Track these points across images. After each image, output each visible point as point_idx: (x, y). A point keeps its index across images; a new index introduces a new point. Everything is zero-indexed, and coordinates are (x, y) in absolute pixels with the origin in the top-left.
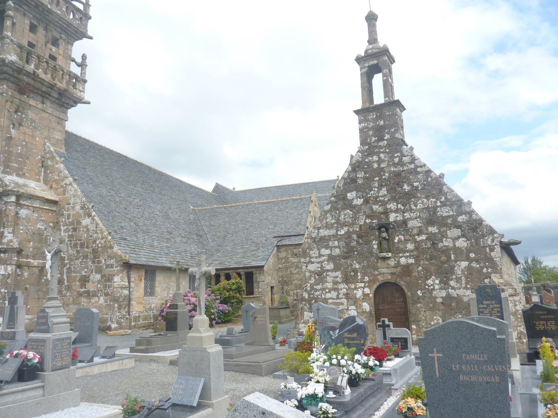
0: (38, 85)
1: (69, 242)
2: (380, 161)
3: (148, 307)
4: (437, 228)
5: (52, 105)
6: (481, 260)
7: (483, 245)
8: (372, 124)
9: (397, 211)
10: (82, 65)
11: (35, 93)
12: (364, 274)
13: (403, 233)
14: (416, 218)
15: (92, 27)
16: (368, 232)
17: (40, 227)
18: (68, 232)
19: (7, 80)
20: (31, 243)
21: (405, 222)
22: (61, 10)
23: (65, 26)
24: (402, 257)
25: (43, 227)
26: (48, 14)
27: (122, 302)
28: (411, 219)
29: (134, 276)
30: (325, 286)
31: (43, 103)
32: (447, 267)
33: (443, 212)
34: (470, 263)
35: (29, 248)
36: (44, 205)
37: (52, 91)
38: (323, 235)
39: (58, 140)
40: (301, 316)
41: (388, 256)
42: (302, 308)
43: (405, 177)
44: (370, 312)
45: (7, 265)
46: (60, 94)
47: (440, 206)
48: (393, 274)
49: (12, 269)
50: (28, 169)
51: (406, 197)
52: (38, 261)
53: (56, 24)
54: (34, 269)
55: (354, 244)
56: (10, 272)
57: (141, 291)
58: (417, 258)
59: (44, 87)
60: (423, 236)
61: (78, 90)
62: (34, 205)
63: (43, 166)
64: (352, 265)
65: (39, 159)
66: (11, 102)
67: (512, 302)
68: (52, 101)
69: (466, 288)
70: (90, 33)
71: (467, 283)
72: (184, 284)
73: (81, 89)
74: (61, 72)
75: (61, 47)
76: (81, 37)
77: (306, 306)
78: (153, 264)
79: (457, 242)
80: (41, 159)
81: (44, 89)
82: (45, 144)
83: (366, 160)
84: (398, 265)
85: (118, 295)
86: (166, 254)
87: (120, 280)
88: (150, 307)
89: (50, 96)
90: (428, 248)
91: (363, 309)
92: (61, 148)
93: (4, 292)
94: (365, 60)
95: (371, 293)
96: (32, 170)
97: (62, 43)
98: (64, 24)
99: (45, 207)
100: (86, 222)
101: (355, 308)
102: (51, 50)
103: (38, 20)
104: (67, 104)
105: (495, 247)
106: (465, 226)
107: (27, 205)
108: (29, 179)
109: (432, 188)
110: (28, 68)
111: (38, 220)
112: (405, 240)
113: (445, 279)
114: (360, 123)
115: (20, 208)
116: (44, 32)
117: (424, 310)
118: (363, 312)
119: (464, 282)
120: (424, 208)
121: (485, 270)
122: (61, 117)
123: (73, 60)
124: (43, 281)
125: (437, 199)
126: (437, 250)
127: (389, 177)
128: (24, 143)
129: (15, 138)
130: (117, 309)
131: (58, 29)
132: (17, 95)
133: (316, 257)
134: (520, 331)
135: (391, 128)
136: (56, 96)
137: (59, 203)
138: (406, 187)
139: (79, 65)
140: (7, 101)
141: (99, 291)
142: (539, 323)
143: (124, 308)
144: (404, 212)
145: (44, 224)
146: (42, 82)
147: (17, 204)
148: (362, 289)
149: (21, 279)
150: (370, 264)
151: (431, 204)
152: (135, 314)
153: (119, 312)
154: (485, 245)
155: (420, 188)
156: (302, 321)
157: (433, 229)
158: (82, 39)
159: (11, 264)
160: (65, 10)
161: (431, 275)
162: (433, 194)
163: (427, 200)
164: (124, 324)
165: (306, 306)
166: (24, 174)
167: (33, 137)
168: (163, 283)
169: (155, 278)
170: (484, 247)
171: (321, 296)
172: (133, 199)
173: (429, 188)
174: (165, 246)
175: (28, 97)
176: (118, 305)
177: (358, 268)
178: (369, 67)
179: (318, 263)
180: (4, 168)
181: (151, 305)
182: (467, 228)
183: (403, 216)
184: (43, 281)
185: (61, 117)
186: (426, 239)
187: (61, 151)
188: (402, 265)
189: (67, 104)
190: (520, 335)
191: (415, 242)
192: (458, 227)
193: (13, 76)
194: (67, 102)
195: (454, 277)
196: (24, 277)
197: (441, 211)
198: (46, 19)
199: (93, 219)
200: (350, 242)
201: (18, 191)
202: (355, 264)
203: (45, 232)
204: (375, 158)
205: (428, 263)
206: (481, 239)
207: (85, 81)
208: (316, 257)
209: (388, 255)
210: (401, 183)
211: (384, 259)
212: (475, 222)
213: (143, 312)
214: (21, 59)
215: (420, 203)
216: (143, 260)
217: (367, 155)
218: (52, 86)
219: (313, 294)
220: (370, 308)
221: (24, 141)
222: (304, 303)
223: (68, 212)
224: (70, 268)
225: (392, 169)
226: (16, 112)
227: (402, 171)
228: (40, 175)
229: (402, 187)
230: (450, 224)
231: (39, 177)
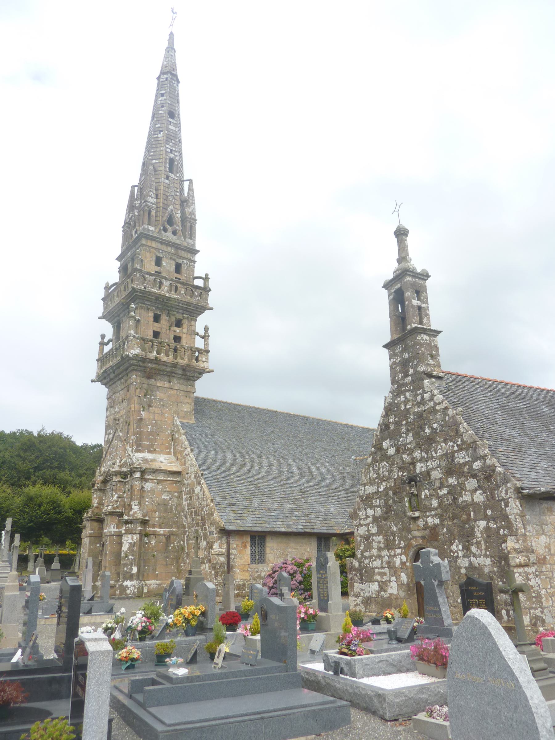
0: (163, 367)
1: (188, 511)
2: (406, 402)
3: (256, 575)
4: (456, 479)
5: (179, 381)
6: (498, 518)
7: (497, 498)
8: (399, 359)
9: (421, 460)
10: (205, 337)
11: (162, 374)
12: (401, 539)
13: (427, 487)
14: (437, 467)
15: (212, 299)
16: (400, 488)
17: (165, 498)
18: (187, 501)
19: (136, 370)
20: (157, 513)
21: (428, 473)
22: (180, 294)
23: (185, 306)
24: (428, 517)
25: (168, 497)
26: (167, 302)
27: (219, 569)
28: (433, 469)
29: (235, 543)
30: (372, 553)
31: (170, 382)
32: (468, 528)
33: (460, 459)
34: (487, 524)
35: (155, 518)
36: (168, 477)
37: (175, 369)
38: (368, 493)
39: (187, 412)
40: (351, 588)
41: (415, 516)
42: (351, 579)
43: (426, 418)
44: (408, 584)
45: (133, 534)
46: (184, 370)
47: (457, 450)
48: (423, 537)
49: (137, 538)
50: (158, 444)
51: (427, 442)
52: (164, 529)
53: (177, 307)
54: (161, 537)
55: (391, 502)
56: (136, 541)
57: (246, 558)
58: (441, 517)
59: (168, 368)
60: (445, 489)
61: (201, 362)
62: (158, 478)
63: (172, 439)
64: (391, 528)
65: (168, 433)
66: (140, 388)
67: (522, 574)
68: (179, 377)
69: (486, 556)
70: (210, 305)
71: (486, 550)
72: (308, 550)
73: (204, 359)
74: (183, 350)
75: (185, 326)
76: (202, 311)
77: (357, 576)
78: (260, 529)
79: (475, 496)
80: (171, 433)
81: (168, 369)
82: (173, 419)
83: (396, 401)
84: (426, 527)
85: (215, 562)
86: (285, 518)
87: (218, 547)
88: (260, 575)
89: (176, 374)
90: (449, 504)
91: (401, 581)
92: (191, 419)
93: (132, 559)
94: (392, 285)
95: (407, 561)
96: (163, 444)
97: (185, 322)
98: (185, 305)
99: (168, 479)
100: (197, 490)
101: (395, 580)
102: (175, 331)
103: (161, 310)
104: (193, 377)
105: (510, 500)
106: (480, 474)
107: (151, 479)
108: (160, 453)
109: (449, 429)
110: (150, 356)
111: (163, 491)
112: (430, 495)
113: (467, 544)
114: (390, 359)
115: (145, 482)
116: (167, 318)
117: (451, 584)
118: (402, 584)
119: (483, 547)
120: (443, 455)
121: (501, 532)
122: (189, 390)
123: (198, 334)
124: (170, 548)
125: (454, 443)
126: (457, 506)
127: (414, 419)
128: (154, 422)
129: (145, 419)
130: (213, 576)
131: (180, 311)
132: (145, 381)
133: (364, 519)
134: (535, 614)
135: (414, 361)
136: (181, 372)
137: (182, 473)
138: (427, 431)
139: (203, 337)
140: (137, 389)
141: (205, 557)
142: (473, 602)
143: (221, 576)
144: (427, 461)
145: (169, 494)
146: (165, 364)
147: (142, 478)
148: (400, 556)
149: (149, 546)
150: (404, 525)
151: (450, 450)
152: (238, 582)
153: (216, 579)
154: (500, 498)
155: (438, 431)
156: (352, 593)
157: (452, 481)
158: (203, 313)
159: (136, 534)
160: (183, 293)
161: (455, 539)
162: (451, 436)
163: (446, 444)
164: (220, 591)
165: (357, 576)
166: (155, 450)
167: (162, 414)
168: (277, 550)
169: (265, 544)
170: (499, 501)
171: (369, 565)
172: (265, 459)
173: (446, 429)
174: (288, 508)
175: (155, 380)
176: (215, 572)
177: (396, 531)
178: (395, 292)
179: (366, 525)
180: (137, 447)
181: (261, 573)
182: (482, 477)
183: (427, 466)
184: (170, 548)
185: (188, 390)
186: (448, 493)
187: (190, 422)
188: (430, 527)
189: (193, 377)
190: (534, 620)
191: (439, 497)
192: (474, 476)
193: (139, 366)
194: (192, 375)
195: (475, 541)
196: (152, 545)
197: (458, 457)
198: (167, 306)
199: (202, 487)
200: (388, 500)
201: (141, 468)
202: (393, 526)
203: (170, 502)
204: (402, 398)
205: (451, 523)
206: (495, 490)
207: (208, 352)
208: (364, 519)
209: (414, 514)
210: (423, 426)
211: (416, 519)
212: (489, 469)
213: (248, 581)
214: (143, 350)
215: (439, 449)
216: (248, 526)
217: (397, 395)
218: (175, 365)
219: (363, 562)
220: (408, 579)
221: (154, 419)
222: (354, 572)
223: (187, 482)
224: (188, 535)
225: (416, 410)
226: (145, 396)
227: (424, 411)
228: (170, 448)
229: (424, 431)
230: (466, 473)
231: (170, 450)
